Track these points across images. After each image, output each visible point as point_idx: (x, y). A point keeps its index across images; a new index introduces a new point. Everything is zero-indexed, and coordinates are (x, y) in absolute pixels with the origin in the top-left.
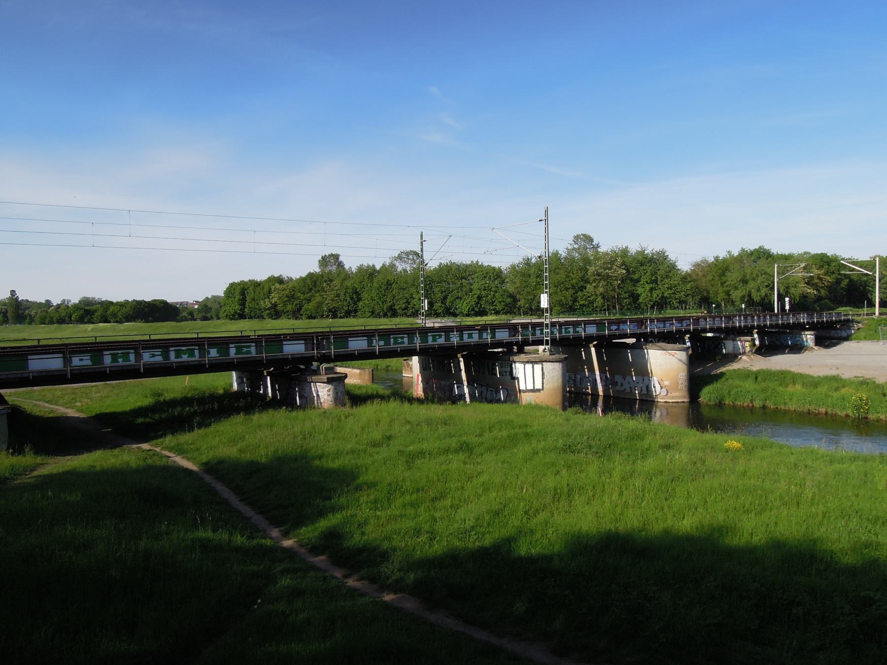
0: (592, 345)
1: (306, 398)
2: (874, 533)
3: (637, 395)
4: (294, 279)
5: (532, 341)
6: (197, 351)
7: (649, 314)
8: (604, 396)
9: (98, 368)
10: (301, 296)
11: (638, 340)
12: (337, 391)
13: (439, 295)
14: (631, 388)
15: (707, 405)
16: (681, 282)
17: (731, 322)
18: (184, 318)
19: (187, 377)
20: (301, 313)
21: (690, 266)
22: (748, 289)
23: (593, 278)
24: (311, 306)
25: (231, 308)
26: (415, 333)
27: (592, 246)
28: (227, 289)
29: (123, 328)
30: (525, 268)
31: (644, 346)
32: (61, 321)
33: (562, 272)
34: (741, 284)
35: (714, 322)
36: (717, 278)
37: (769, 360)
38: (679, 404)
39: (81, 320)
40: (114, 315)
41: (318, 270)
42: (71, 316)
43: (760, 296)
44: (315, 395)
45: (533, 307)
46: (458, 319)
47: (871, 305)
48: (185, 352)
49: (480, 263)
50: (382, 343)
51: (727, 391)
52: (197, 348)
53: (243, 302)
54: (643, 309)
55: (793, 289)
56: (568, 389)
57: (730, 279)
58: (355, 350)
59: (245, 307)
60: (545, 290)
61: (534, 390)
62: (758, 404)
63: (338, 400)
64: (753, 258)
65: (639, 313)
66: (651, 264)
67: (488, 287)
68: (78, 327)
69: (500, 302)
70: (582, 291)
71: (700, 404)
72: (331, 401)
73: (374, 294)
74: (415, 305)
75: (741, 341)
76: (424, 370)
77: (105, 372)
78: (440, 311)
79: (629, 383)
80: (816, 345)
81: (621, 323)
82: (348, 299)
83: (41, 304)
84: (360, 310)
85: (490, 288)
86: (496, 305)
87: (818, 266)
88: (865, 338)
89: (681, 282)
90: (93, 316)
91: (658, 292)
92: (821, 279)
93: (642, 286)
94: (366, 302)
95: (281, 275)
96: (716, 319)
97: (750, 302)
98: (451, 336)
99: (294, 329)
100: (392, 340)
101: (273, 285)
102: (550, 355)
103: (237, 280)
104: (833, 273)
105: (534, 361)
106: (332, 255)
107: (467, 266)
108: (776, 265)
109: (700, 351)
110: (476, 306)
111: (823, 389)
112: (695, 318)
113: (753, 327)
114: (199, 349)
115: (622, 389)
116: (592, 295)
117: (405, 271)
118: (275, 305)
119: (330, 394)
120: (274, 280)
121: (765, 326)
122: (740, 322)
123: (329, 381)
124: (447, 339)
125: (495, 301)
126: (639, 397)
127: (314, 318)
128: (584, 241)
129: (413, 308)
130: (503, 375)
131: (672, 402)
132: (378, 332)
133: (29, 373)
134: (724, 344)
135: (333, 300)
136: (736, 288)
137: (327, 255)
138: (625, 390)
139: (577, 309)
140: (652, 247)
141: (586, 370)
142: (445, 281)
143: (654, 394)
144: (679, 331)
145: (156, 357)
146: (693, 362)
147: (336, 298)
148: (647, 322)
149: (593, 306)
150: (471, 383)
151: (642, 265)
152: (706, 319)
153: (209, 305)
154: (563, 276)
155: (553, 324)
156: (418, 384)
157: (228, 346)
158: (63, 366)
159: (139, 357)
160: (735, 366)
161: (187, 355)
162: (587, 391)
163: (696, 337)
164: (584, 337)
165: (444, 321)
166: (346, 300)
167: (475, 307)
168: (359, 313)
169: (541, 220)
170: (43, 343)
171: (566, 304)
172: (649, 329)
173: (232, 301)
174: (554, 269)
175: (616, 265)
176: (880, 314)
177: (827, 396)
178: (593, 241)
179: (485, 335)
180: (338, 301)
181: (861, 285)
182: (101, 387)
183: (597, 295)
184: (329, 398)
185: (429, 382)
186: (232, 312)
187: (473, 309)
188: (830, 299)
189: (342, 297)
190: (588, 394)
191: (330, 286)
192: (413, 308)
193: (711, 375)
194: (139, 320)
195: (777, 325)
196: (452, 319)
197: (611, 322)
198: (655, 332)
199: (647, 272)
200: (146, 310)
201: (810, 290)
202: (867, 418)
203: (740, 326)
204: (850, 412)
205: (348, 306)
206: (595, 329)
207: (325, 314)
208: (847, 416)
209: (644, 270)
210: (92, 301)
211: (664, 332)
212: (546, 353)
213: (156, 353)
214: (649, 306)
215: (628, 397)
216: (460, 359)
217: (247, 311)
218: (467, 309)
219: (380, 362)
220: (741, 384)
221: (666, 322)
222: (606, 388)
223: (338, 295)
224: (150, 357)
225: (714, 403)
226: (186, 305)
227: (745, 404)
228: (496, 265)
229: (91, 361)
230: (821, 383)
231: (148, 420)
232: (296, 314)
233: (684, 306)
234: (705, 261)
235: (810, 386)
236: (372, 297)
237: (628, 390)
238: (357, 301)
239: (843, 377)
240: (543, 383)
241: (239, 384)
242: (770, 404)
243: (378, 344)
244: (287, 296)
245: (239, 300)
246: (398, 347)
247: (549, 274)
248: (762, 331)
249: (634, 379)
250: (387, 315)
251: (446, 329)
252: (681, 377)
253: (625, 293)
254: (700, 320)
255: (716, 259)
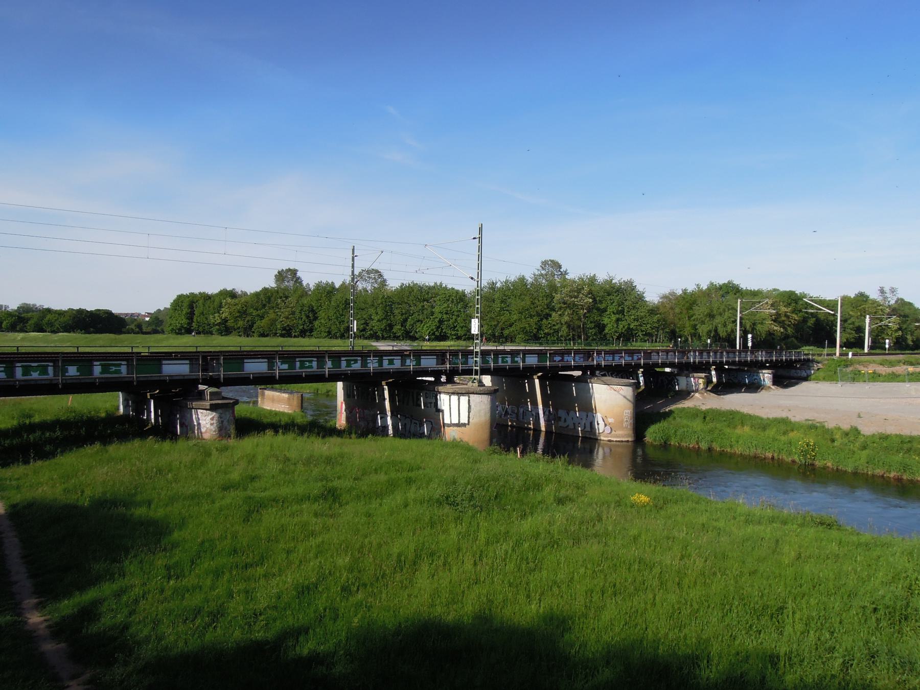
1: (187, 426)
2: (755, 629)
4: (249, 294)
5: (462, 370)
6: (316, 362)
8: (546, 432)
9: (151, 376)
11: (584, 373)
12: (222, 420)
14: (574, 424)
15: (652, 445)
16: (647, 314)
17: (685, 358)
21: (659, 298)
22: (714, 324)
23: (559, 305)
24: (264, 323)
26: (324, 357)
28: (174, 301)
29: (56, 338)
33: (527, 298)
34: (708, 319)
35: (667, 356)
36: (684, 312)
37: (723, 398)
40: (50, 324)
41: (273, 285)
43: (727, 331)
44: (196, 424)
47: (833, 344)
48: (35, 369)
49: (444, 285)
50: (285, 366)
51: (673, 431)
53: (191, 316)
54: (609, 340)
55: (759, 325)
56: (510, 423)
57: (697, 313)
58: (250, 374)
59: (193, 322)
60: (476, 315)
61: (459, 425)
62: (704, 446)
63: (222, 431)
64: (721, 292)
69: (462, 327)
70: (547, 319)
71: (645, 444)
72: (215, 431)
73: (331, 313)
75: (695, 378)
77: (302, 376)
78: (400, 334)
80: (774, 384)
81: (566, 354)
82: (304, 317)
86: (457, 330)
87: (785, 304)
88: (824, 379)
90: (27, 325)
92: (788, 317)
94: (323, 321)
95: (234, 289)
96: (670, 354)
97: (716, 338)
98: (368, 361)
100: (298, 364)
101: (224, 299)
102: (479, 386)
103: (186, 292)
104: (800, 311)
106: (290, 270)
107: (430, 288)
108: (739, 300)
110: (437, 330)
111: (771, 432)
113: (638, 366)
115: (565, 425)
116: (557, 324)
117: (365, 290)
118: (225, 321)
120: (225, 293)
121: (721, 362)
122: (695, 358)
123: (213, 408)
124: (364, 364)
127: (267, 336)
129: (371, 329)
130: (428, 407)
131: (616, 441)
134: (678, 380)
135: (287, 318)
136: (703, 323)
137: (284, 269)
138: (568, 426)
139: (542, 337)
140: (620, 276)
141: (529, 403)
142: (406, 303)
144: (628, 365)
146: (640, 399)
150: (395, 413)
151: (609, 295)
153: (161, 318)
154: (529, 303)
156: (341, 413)
160: (687, 404)
161: (38, 372)
163: (650, 371)
168: (314, 333)
169: (474, 238)
170: (23, 350)
171: (531, 332)
173: (179, 314)
176: (841, 355)
177: (774, 439)
178: (561, 268)
179: (408, 361)
180: (293, 319)
181: (827, 325)
183: (562, 324)
186: (179, 326)
188: (796, 338)
189: (297, 315)
190: (530, 429)
192: (371, 329)
194: (79, 331)
195: (734, 363)
196: (409, 342)
197: (556, 353)
198: (602, 365)
199: (613, 302)
201: (777, 328)
202: (813, 465)
203: (694, 362)
204: (796, 458)
205: (304, 325)
208: (794, 462)
210: (32, 308)
212: (474, 384)
214: (615, 337)
215: (571, 434)
217: (195, 326)
219: (321, 386)
220: (689, 424)
223: (293, 313)
227: (691, 446)
228: (459, 288)
230: (769, 425)
232: (247, 331)
234: (673, 294)
235: (759, 428)
236: (329, 316)
237: (571, 426)
239: (793, 420)
240: (469, 417)
241: (125, 407)
242: (717, 447)
244: (239, 312)
246: (302, 372)
248: (720, 369)
250: (344, 336)
253: (591, 322)
255: (685, 291)
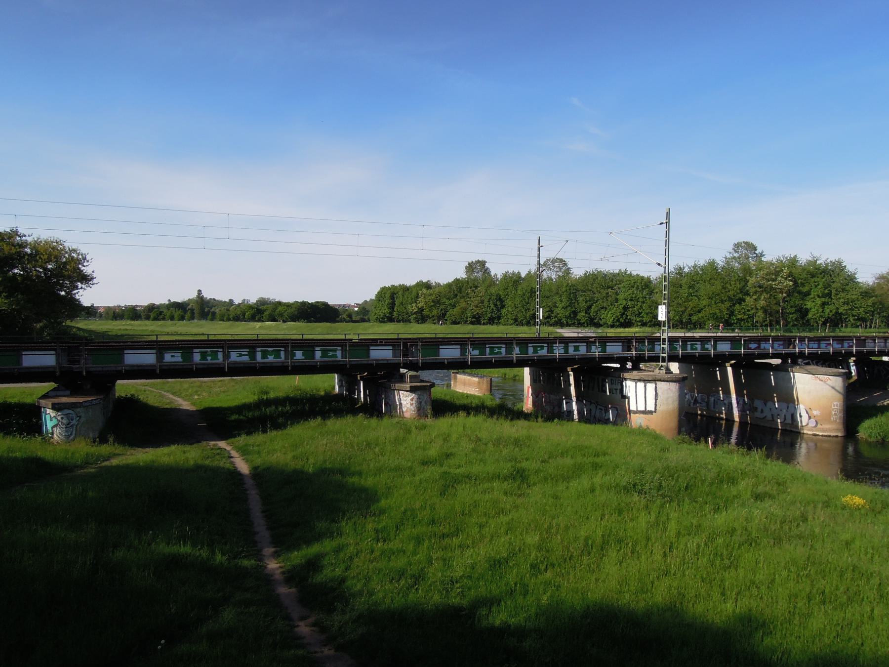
0: (729, 364)
3: (779, 424)
4: (442, 284)
5: (648, 357)
6: (284, 352)
7: (819, 332)
8: (741, 423)
9: (187, 365)
10: (447, 301)
11: (784, 361)
13: (583, 305)
14: (772, 415)
15: (866, 441)
16: (860, 297)
18: (343, 320)
19: (297, 377)
20: (446, 318)
21: (874, 279)
23: (754, 289)
25: (381, 312)
26: (512, 344)
27: (755, 255)
28: (378, 293)
30: (677, 277)
31: (790, 369)
32: (237, 319)
38: (831, 438)
39: (253, 318)
40: (281, 315)
41: (464, 276)
42: (244, 315)
44: (398, 403)
45: (684, 320)
46: (600, 330)
48: (271, 353)
50: (476, 352)
52: (283, 349)
53: (392, 306)
58: (445, 359)
59: (394, 311)
60: (663, 301)
61: (645, 412)
63: (420, 411)
65: (807, 330)
66: (824, 276)
67: (635, 297)
68: (249, 325)
69: (647, 314)
70: (740, 304)
72: (414, 411)
73: (518, 300)
74: (558, 314)
76: (534, 382)
78: (584, 321)
79: (771, 409)
82: (492, 306)
83: (225, 302)
84: (503, 317)
85: (637, 298)
89: (860, 297)
91: (831, 307)
93: (812, 300)
94: (510, 309)
95: (429, 281)
98: (554, 348)
99: (436, 334)
100: (488, 350)
102: (666, 373)
105: (647, 379)
106: (478, 262)
107: (614, 275)
109: (867, 377)
112: (747, 339)
114: (285, 351)
115: (762, 416)
116: (752, 309)
117: (550, 279)
118: (421, 310)
119: (413, 404)
123: (413, 390)
124: (550, 350)
125: (642, 313)
126: (781, 426)
127: (459, 323)
128: (746, 249)
129: (556, 317)
130: (613, 393)
131: (822, 436)
132: (471, 341)
133: (193, 364)
135: (477, 306)
138: (766, 417)
139: (734, 323)
140: (826, 256)
141: (721, 392)
142: (590, 290)
143: (800, 424)
144: (837, 353)
145: (243, 357)
146: (851, 391)
147: (480, 304)
148: (796, 340)
149: (753, 321)
150: (580, 399)
151: (813, 276)
152: (875, 340)
153: (367, 308)
154: (719, 287)
155: (672, 340)
156: (528, 396)
157: (314, 348)
158: (392, 356)
159: (227, 356)
162: (721, 416)
164: (856, 352)
165: (584, 331)
166: (490, 306)
167: (621, 318)
168: (502, 321)
169: (661, 224)
172: (797, 350)
174: (708, 279)
175: (782, 276)
182: (227, 382)
183: (757, 309)
184: (412, 407)
185: (539, 395)
186: (382, 315)
187: (618, 320)
190: (722, 419)
191: (475, 293)
192: (556, 317)
193: (877, 406)
196: (593, 329)
199: (818, 285)
200: (309, 311)
206: (729, 346)
207: (468, 320)
209: (815, 282)
210: (267, 301)
211: (818, 353)
212: (661, 371)
213: (243, 353)
214: (820, 323)
216: (570, 373)
218: (611, 320)
221: (822, 342)
222: (743, 413)
223: (482, 302)
224: (238, 356)
225: (875, 440)
226: (348, 307)
228: (644, 274)
229: (182, 358)
231: (241, 417)
233: (868, 324)
236: (515, 305)
237: (769, 417)
238: (501, 308)
240: (656, 405)
243: (470, 353)
244: (433, 301)
245: (389, 304)
246: (492, 358)
247: (668, 283)
249: (777, 406)
251: (569, 339)
252: (834, 406)
253: (791, 307)
254: (867, 341)
